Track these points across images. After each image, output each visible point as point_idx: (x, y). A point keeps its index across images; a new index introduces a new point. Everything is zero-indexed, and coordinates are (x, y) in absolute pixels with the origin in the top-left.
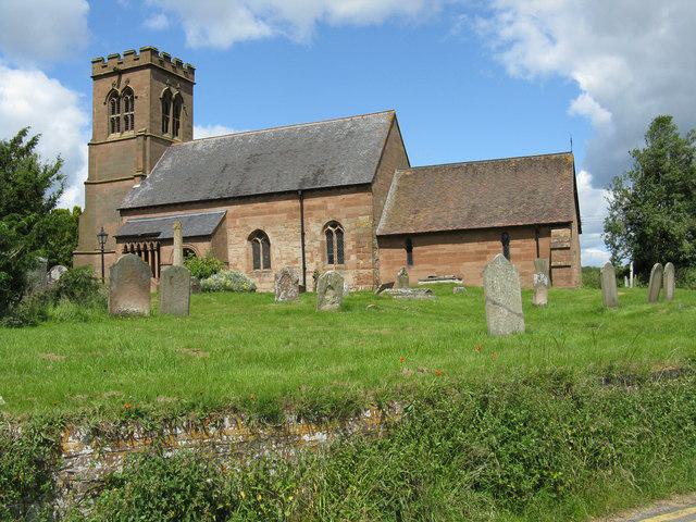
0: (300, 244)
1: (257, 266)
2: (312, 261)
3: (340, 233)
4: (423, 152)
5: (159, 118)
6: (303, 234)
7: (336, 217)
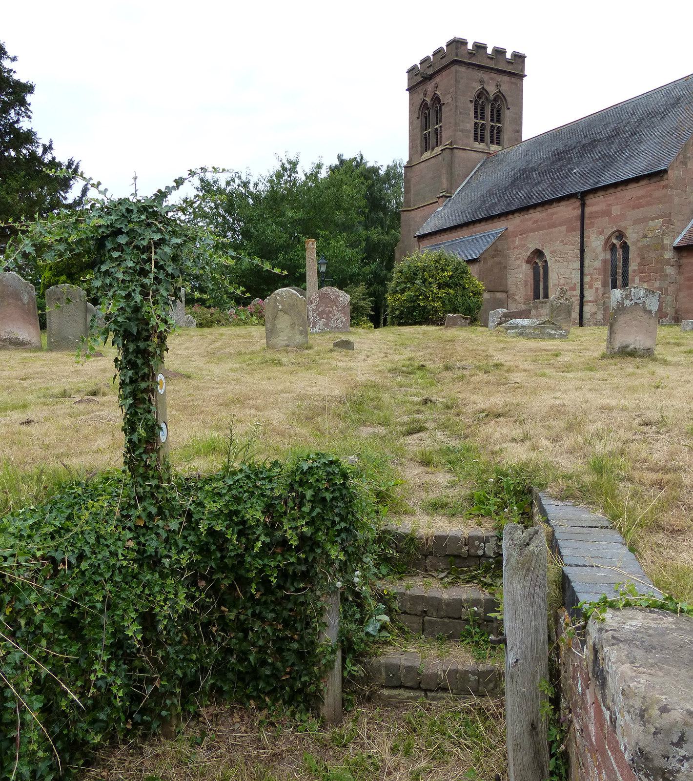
0: (577, 265)
1: (536, 296)
2: (591, 287)
3: (625, 247)
6: (582, 251)
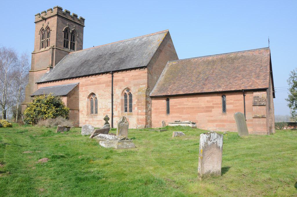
0: (111, 101)
1: (92, 112)
2: (116, 110)
4: (184, 50)
5: (62, 41)
6: (112, 95)
7: (129, 86)
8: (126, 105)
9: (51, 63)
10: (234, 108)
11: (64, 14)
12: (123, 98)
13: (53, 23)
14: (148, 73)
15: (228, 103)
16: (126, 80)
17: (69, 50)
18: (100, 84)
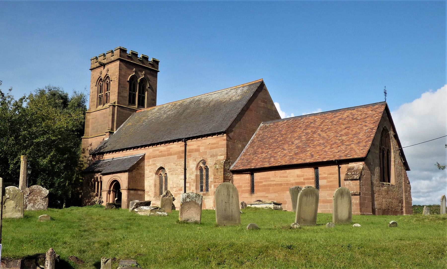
0: (183, 177)
5: (127, 94)
6: (185, 169)
8: (202, 182)
9: (110, 126)
10: (328, 184)
11: (129, 57)
12: (199, 173)
13: (114, 70)
14: (227, 140)
15: (321, 177)
16: (202, 149)
17: (136, 106)
18: (170, 154)
